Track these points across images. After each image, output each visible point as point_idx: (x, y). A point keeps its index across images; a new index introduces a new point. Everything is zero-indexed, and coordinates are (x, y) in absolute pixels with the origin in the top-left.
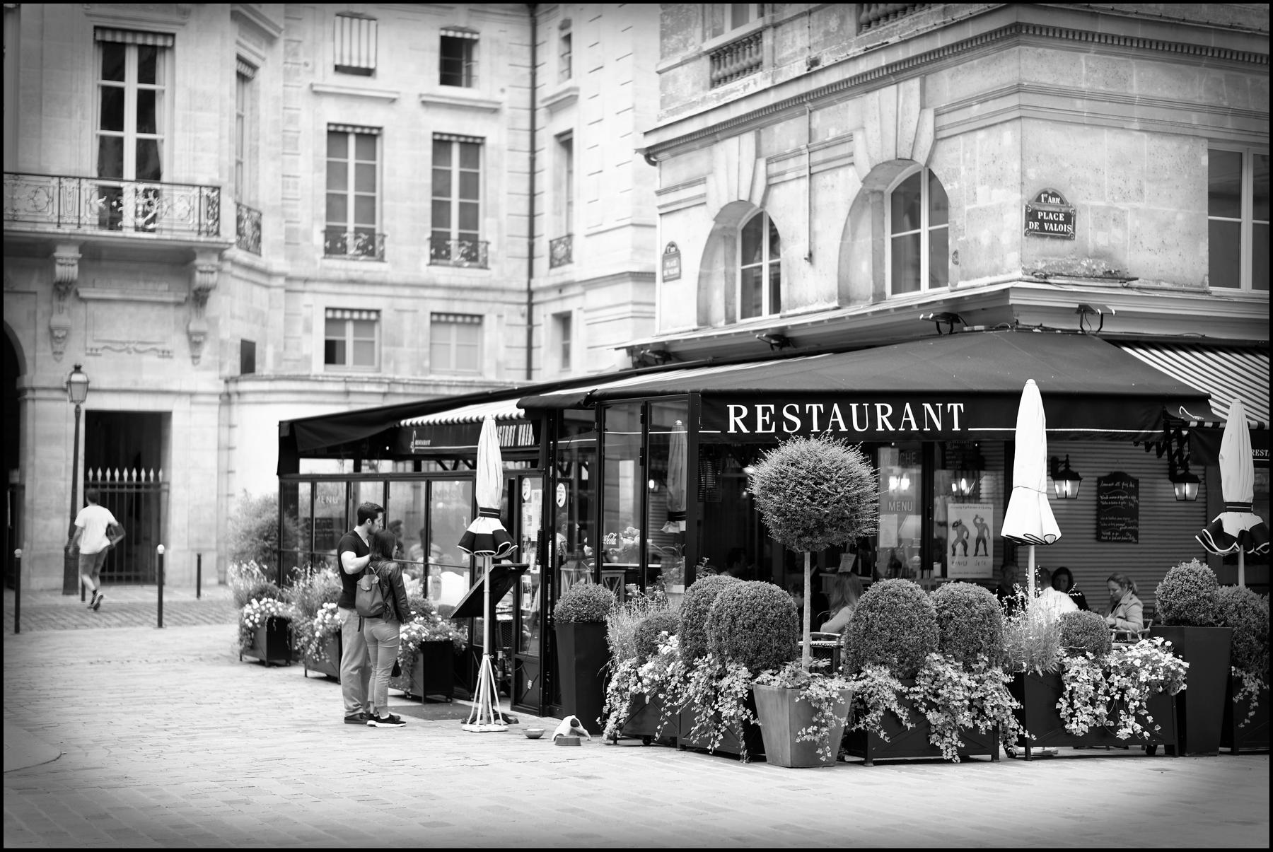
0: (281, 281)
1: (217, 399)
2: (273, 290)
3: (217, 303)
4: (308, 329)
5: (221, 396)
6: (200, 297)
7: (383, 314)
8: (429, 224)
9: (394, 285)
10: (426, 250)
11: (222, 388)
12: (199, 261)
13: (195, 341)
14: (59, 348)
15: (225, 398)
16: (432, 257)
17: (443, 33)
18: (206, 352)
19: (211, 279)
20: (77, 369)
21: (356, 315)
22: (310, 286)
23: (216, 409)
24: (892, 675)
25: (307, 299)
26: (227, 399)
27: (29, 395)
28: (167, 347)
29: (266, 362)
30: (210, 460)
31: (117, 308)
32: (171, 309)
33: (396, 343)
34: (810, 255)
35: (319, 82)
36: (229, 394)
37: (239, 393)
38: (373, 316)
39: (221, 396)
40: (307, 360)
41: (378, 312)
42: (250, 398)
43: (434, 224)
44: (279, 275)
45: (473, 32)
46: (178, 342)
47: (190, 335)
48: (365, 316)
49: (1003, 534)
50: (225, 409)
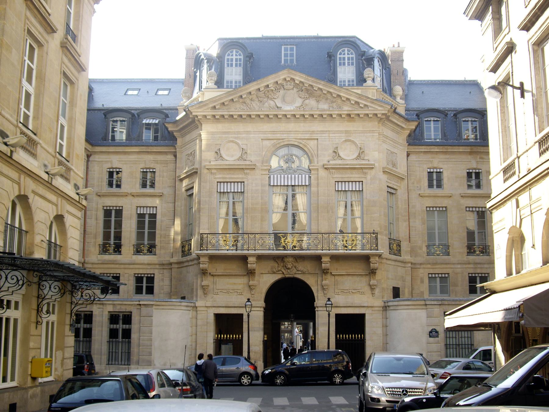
0: (410, 265)
1: (381, 309)
2: (407, 268)
3: (379, 275)
4: (422, 282)
5: (383, 307)
6: (373, 272)
7: (450, 275)
8: (466, 240)
9: (454, 264)
10: (465, 250)
11: (383, 304)
12: (372, 260)
13: (372, 288)
14: (325, 292)
15: (384, 308)
16: (468, 252)
17: (468, 171)
18: (377, 291)
19: (376, 266)
20: (329, 299)
21: (440, 276)
22: (422, 266)
23: (381, 312)
24: (301, 347)
25: (421, 271)
26: (385, 308)
27: (316, 309)
28: (363, 290)
29: (405, 293)
30: (380, 331)
31: (345, 278)
32: (364, 277)
33: (456, 285)
34: (534, 245)
35: (422, 192)
36: (386, 307)
37: (388, 306)
38: (447, 275)
39: (383, 307)
40: (422, 293)
41: (488, 274)
42: (391, 308)
43: (468, 240)
44: (409, 263)
45: (479, 169)
46: (367, 289)
47: (370, 285)
48: (433, 276)
49: (446, 327)
50: (384, 312)
